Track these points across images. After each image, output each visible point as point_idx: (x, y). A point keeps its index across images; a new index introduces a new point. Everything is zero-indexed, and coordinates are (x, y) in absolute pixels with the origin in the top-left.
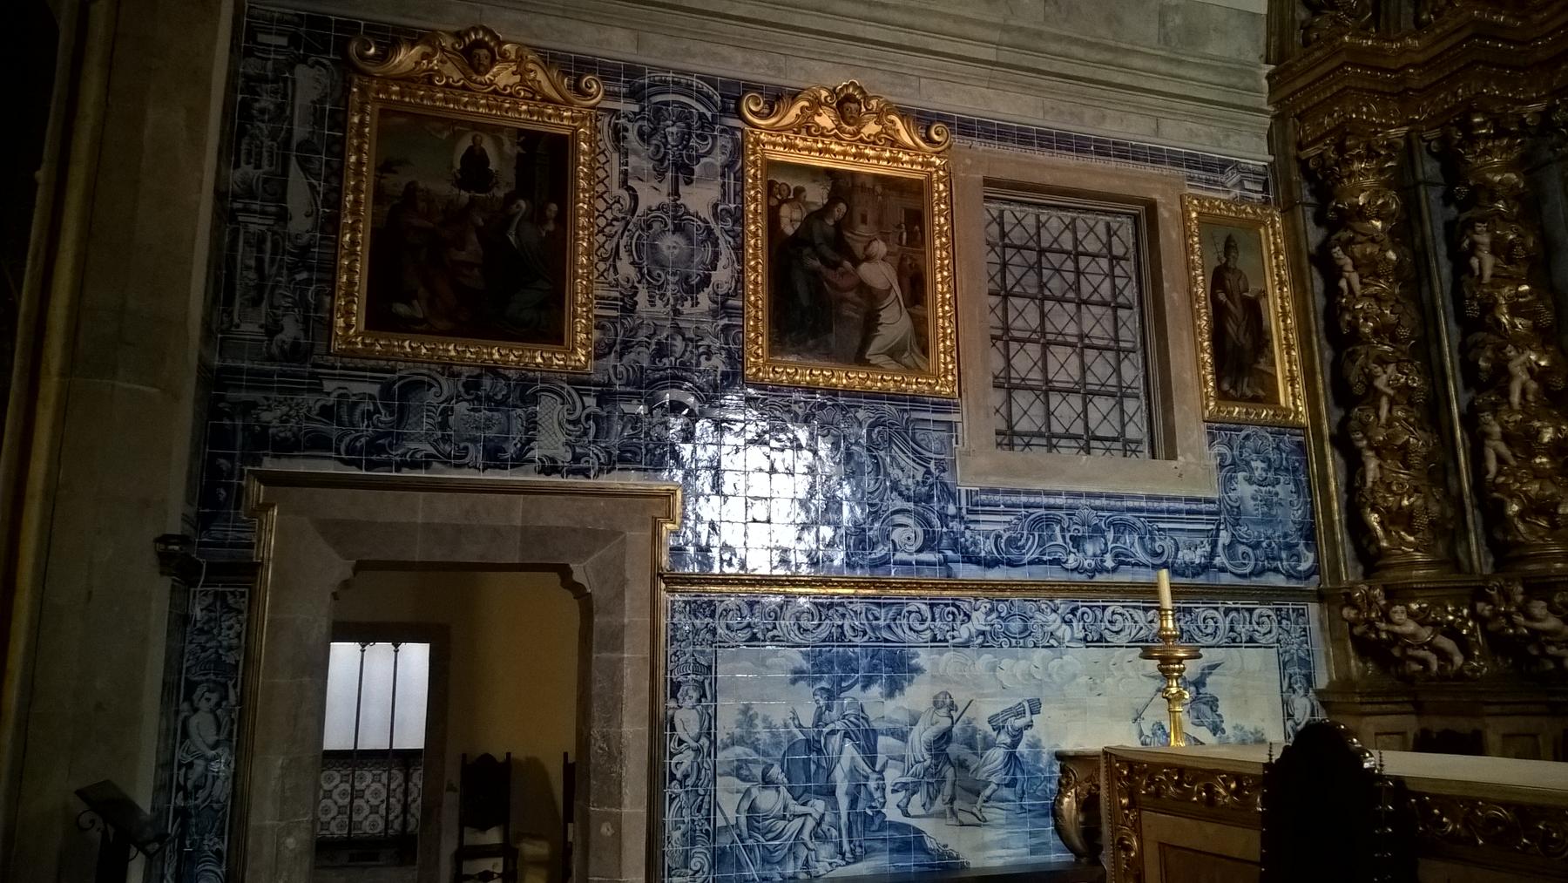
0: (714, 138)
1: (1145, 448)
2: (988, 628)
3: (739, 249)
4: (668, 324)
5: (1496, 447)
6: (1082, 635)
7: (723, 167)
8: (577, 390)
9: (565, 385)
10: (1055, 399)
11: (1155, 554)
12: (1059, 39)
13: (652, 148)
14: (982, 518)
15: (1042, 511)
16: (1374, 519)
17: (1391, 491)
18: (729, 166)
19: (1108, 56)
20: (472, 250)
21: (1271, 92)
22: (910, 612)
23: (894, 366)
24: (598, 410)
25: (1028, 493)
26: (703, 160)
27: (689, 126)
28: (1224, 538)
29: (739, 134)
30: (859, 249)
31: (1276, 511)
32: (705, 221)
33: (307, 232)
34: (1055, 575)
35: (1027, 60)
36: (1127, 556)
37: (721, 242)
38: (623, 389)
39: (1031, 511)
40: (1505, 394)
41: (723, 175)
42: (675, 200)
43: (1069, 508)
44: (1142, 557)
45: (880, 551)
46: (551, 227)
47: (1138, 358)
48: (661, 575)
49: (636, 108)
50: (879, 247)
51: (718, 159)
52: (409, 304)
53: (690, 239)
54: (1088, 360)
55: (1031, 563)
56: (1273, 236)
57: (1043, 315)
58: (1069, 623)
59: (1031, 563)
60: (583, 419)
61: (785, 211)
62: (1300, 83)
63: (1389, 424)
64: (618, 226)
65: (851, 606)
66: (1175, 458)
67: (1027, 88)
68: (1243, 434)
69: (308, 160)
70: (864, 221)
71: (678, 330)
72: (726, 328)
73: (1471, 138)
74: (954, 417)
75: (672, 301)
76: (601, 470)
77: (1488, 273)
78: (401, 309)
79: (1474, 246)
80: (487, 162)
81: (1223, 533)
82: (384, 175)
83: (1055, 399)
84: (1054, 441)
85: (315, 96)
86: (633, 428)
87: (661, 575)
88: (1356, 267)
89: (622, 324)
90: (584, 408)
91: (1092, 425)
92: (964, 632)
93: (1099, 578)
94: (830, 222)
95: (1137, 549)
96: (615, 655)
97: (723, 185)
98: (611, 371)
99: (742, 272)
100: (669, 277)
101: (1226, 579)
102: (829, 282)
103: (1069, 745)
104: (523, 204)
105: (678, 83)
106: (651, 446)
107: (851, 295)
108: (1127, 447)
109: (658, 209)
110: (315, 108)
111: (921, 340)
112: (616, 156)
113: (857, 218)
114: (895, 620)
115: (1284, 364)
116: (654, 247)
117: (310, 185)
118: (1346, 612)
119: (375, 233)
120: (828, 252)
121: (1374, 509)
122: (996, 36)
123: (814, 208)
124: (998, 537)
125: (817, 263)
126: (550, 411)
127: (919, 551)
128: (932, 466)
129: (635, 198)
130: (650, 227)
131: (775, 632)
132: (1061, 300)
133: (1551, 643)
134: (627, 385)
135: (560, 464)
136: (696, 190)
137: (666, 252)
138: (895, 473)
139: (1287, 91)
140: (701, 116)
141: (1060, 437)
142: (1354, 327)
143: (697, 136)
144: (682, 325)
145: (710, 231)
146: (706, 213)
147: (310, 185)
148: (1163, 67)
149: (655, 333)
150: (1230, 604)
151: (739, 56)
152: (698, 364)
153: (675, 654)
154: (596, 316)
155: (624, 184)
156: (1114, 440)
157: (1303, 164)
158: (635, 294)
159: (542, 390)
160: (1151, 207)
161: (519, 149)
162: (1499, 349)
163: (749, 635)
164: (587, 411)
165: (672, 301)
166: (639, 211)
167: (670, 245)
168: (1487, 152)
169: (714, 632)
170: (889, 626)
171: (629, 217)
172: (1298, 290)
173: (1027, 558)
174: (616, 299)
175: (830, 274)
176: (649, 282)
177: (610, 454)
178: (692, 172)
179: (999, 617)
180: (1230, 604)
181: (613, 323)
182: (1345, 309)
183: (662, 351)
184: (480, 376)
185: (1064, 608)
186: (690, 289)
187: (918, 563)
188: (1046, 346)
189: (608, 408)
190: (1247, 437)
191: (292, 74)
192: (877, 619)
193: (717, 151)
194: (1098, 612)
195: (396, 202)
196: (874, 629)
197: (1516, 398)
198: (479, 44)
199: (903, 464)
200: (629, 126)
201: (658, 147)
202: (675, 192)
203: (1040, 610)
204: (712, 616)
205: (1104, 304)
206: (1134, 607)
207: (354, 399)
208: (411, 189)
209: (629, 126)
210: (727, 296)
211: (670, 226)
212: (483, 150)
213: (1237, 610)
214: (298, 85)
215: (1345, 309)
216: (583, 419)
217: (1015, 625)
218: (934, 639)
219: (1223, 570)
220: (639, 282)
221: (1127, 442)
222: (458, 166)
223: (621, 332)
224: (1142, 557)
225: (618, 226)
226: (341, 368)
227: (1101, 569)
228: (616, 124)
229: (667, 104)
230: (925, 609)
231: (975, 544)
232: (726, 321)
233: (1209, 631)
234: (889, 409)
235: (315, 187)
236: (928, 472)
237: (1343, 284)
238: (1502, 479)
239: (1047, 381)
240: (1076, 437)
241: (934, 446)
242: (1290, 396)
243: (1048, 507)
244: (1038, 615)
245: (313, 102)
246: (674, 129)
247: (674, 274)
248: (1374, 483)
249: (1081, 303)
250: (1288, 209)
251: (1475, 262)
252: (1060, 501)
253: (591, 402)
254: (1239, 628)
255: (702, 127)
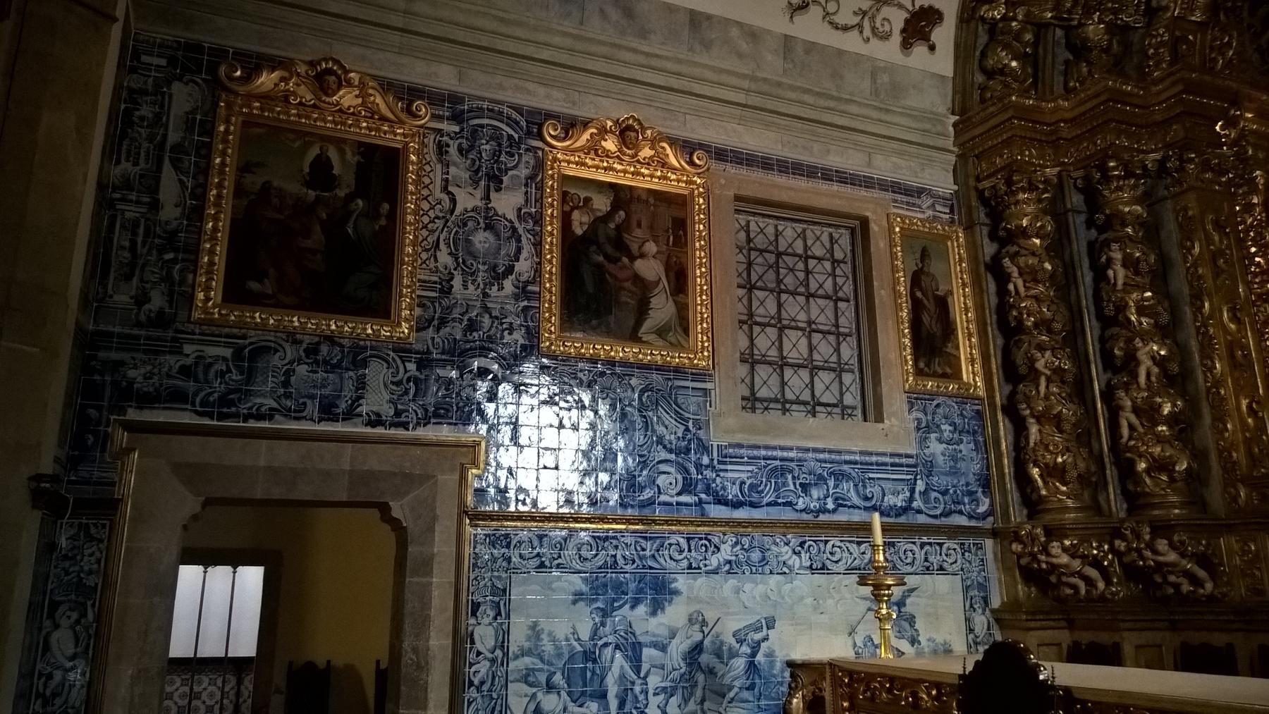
0: (520, 155)
1: (859, 412)
2: (734, 558)
3: (538, 245)
4: (478, 304)
5: (1127, 417)
6: (808, 564)
7: (527, 179)
8: (400, 357)
9: (391, 353)
10: (788, 372)
11: (866, 499)
12: (793, 88)
13: (469, 162)
14: (729, 467)
15: (778, 463)
16: (1035, 472)
17: (1048, 451)
18: (531, 178)
19: (832, 104)
20: (316, 239)
21: (956, 137)
22: (670, 545)
23: (661, 343)
24: (417, 374)
25: (767, 448)
26: (510, 173)
27: (500, 145)
28: (920, 486)
29: (540, 153)
30: (634, 248)
31: (962, 465)
32: (511, 222)
33: (176, 219)
34: (788, 515)
35: (770, 104)
36: (844, 499)
37: (524, 240)
38: (439, 356)
39: (768, 462)
40: (1135, 376)
41: (526, 185)
42: (487, 204)
43: (799, 460)
44: (856, 500)
45: (647, 494)
46: (383, 222)
47: (853, 341)
48: (466, 512)
49: (457, 129)
50: (651, 247)
51: (523, 172)
52: (260, 281)
53: (497, 235)
54: (814, 342)
55: (769, 504)
56: (957, 247)
57: (780, 305)
58: (798, 554)
59: (769, 504)
60: (404, 381)
61: (576, 215)
62: (977, 131)
63: (1047, 398)
64: (439, 223)
65: (622, 539)
66: (879, 419)
67: (768, 125)
68: (935, 403)
69: (179, 160)
70: (639, 225)
71: (486, 309)
72: (526, 309)
73: (1107, 179)
74: (708, 386)
75: (482, 286)
76: (418, 424)
77: (1120, 282)
78: (254, 286)
79: (1110, 260)
80: (332, 167)
81: (919, 482)
82: (246, 175)
83: (788, 372)
84: (788, 406)
85: (188, 107)
86: (447, 389)
87: (466, 512)
88: (1021, 274)
89: (440, 303)
90: (406, 372)
91: (817, 394)
92: (714, 561)
93: (822, 517)
94: (612, 226)
95: (852, 493)
96: (424, 580)
97: (526, 193)
98: (430, 342)
99: (540, 263)
100: (480, 266)
101: (922, 519)
102: (610, 274)
103: (798, 655)
104: (360, 202)
105: (492, 110)
106: (461, 404)
107: (627, 285)
108: (845, 412)
109: (473, 211)
110: (188, 118)
111: (683, 322)
112: (439, 166)
113: (634, 223)
114: (658, 551)
115: (966, 348)
116: (468, 241)
117: (180, 180)
118: (1014, 546)
119: (234, 223)
120: (609, 249)
121: (1036, 465)
122: (746, 84)
123: (599, 214)
124: (743, 483)
125: (601, 258)
126: (377, 373)
127: (679, 494)
128: (690, 425)
129: (454, 201)
130: (465, 225)
131: (560, 561)
132: (794, 293)
133: (1171, 573)
134: (442, 353)
135: (384, 418)
136: (504, 197)
137: (478, 246)
138: (661, 430)
139: (967, 137)
140: (510, 137)
141: (792, 403)
142: (1020, 321)
143: (506, 153)
144: (489, 305)
145: (514, 230)
146: (512, 215)
147: (180, 180)
148: (874, 114)
149: (467, 311)
150: (925, 539)
151: (542, 91)
152: (502, 337)
153: (476, 579)
154: (418, 296)
155: (445, 189)
156: (835, 406)
157: (980, 193)
158: (452, 279)
159: (371, 356)
160: (865, 222)
161: (357, 158)
162: (1130, 341)
163: (538, 563)
164: (408, 375)
165: (482, 286)
166: (457, 212)
167: (482, 240)
168: (1119, 189)
169: (509, 560)
170: (653, 556)
171: (448, 216)
172: (977, 290)
173: (765, 500)
174: (435, 283)
175: (611, 267)
176: (463, 270)
177: (426, 411)
178: (501, 182)
179: (742, 549)
180: (925, 539)
181: (433, 303)
182: (1012, 307)
183: (472, 326)
184: (318, 343)
185: (794, 542)
186: (497, 277)
187: (678, 504)
188: (781, 330)
189: (426, 372)
190: (938, 406)
191: (170, 89)
192: (644, 550)
193: (522, 165)
194: (822, 545)
195: (253, 197)
196: (641, 558)
197: (1142, 379)
198: (329, 72)
199: (667, 423)
200: (451, 142)
201: (473, 161)
202: (487, 198)
203: (776, 544)
204: (508, 546)
205: (827, 297)
206: (850, 542)
207: (210, 360)
208: (266, 187)
209: (451, 142)
210: (527, 283)
211: (482, 225)
212: (328, 159)
213: (930, 544)
214: (174, 97)
215: (1012, 307)
216: (404, 381)
217: (756, 556)
218: (690, 567)
219: (919, 512)
220: (455, 269)
221: (844, 408)
222: (307, 170)
223: (439, 310)
224: (856, 500)
225: (439, 223)
226: (200, 334)
227: (824, 510)
228: (440, 141)
229: (482, 126)
230: (683, 542)
231: (724, 488)
232: (525, 303)
233: (909, 560)
234: (656, 377)
235: (184, 182)
236: (687, 429)
237: (1011, 287)
238: (1132, 443)
239: (782, 358)
240: (805, 403)
241: (692, 409)
242: (971, 374)
243: (782, 459)
244: (773, 547)
245: (187, 113)
246: (488, 147)
247: (484, 264)
248: (1035, 444)
249: (809, 296)
250: (969, 228)
251: (1110, 273)
252: (792, 454)
253: (412, 367)
254: (931, 559)
255: (511, 146)
